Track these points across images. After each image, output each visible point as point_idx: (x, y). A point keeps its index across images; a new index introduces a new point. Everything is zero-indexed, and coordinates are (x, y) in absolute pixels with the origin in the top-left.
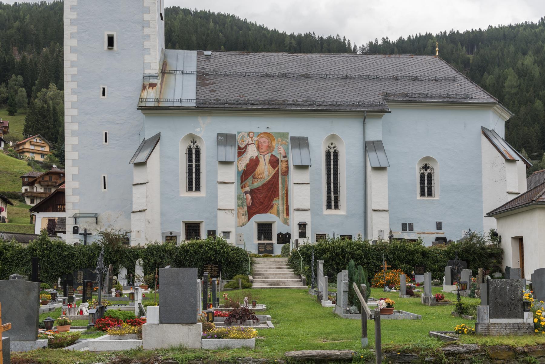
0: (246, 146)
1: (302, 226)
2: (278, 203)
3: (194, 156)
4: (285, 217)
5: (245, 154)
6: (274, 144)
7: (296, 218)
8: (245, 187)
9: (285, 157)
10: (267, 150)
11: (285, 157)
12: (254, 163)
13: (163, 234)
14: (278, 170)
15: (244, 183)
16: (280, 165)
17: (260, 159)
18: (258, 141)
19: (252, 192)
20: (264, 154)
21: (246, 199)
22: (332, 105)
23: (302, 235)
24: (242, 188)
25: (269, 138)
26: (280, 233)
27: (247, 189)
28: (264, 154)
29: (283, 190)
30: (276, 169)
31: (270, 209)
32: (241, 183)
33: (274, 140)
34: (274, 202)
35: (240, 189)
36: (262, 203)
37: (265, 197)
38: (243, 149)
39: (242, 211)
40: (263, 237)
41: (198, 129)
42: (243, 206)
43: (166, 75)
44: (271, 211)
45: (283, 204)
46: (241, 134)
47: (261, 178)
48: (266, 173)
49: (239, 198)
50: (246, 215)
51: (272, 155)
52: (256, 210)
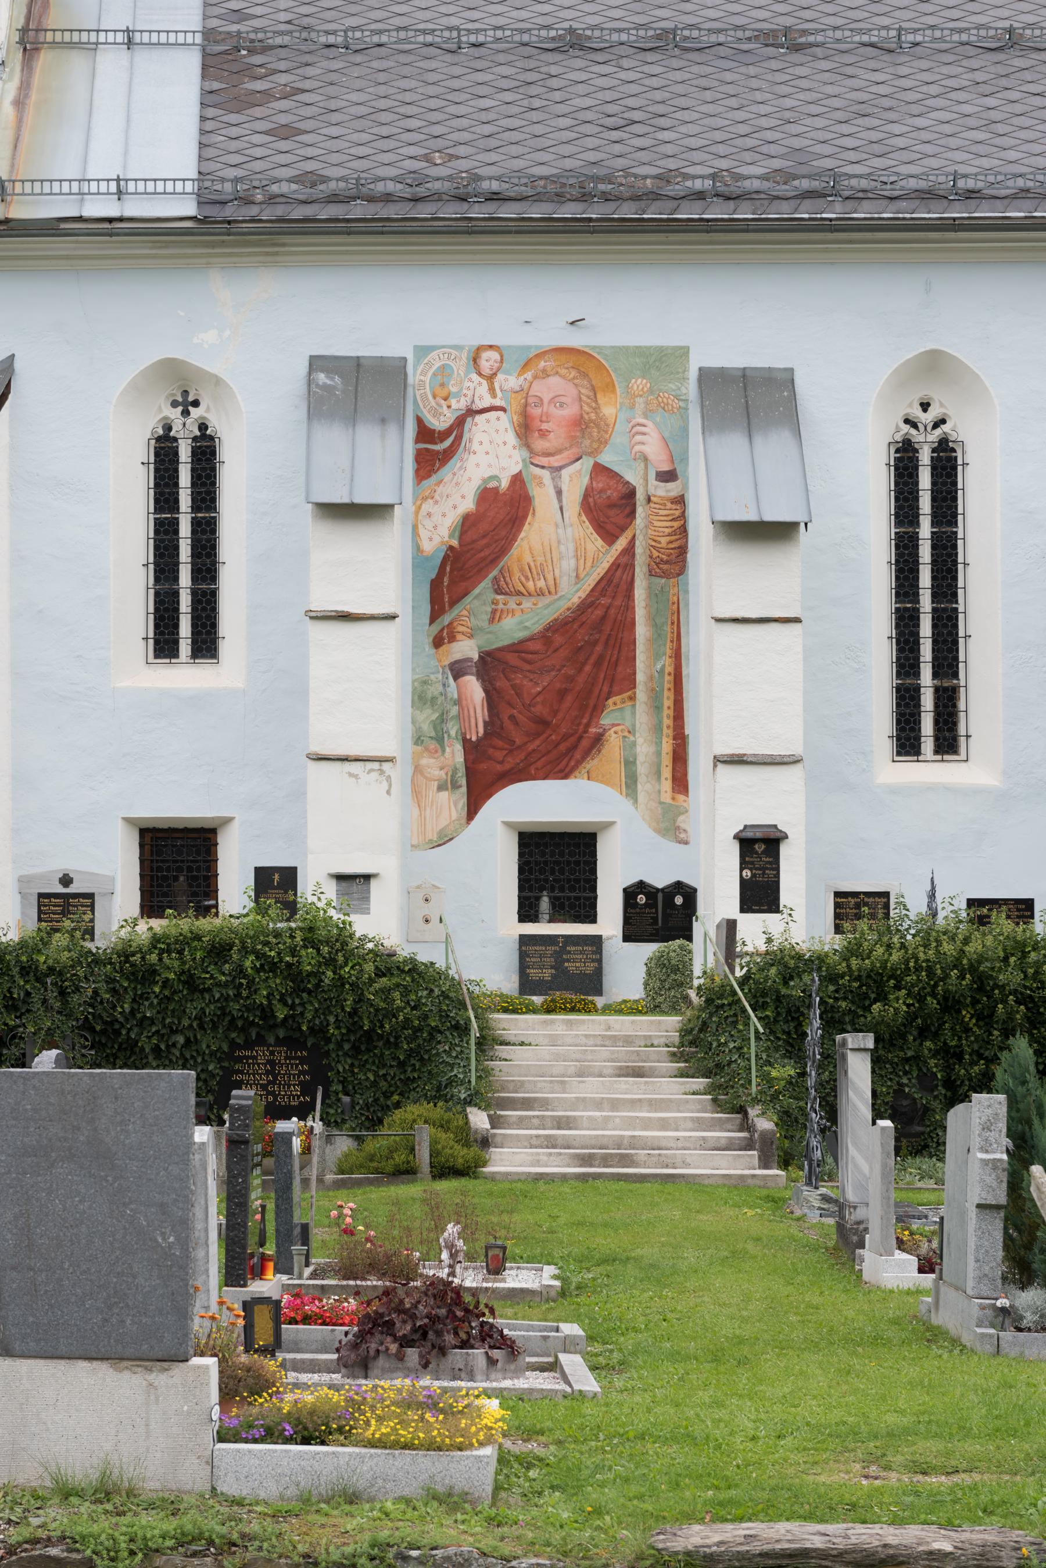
0: (460, 423)
1: (760, 849)
2: (630, 725)
3: (185, 478)
4: (667, 796)
5: (454, 463)
6: (608, 411)
7: (729, 803)
8: (452, 639)
9: (668, 476)
10: (573, 441)
11: (668, 476)
12: (502, 514)
13: (24, 881)
15: (446, 619)
17: (534, 491)
19: (490, 666)
20: (555, 461)
21: (459, 702)
22: (928, 195)
23: (760, 893)
24: (438, 642)
25: (585, 375)
26: (641, 886)
27: (466, 649)
28: (555, 461)
30: (621, 543)
31: (587, 753)
32: (433, 620)
33: (610, 387)
34: (605, 720)
35: (429, 650)
36: (543, 723)
37: (562, 694)
38: (447, 433)
39: (434, 768)
41: (210, 337)
42: (440, 739)
43: (44, 58)
44: (590, 764)
45: (657, 729)
47: (540, 593)
48: (568, 565)
49: (421, 698)
50: (455, 786)
51: (600, 470)
52: (510, 762)
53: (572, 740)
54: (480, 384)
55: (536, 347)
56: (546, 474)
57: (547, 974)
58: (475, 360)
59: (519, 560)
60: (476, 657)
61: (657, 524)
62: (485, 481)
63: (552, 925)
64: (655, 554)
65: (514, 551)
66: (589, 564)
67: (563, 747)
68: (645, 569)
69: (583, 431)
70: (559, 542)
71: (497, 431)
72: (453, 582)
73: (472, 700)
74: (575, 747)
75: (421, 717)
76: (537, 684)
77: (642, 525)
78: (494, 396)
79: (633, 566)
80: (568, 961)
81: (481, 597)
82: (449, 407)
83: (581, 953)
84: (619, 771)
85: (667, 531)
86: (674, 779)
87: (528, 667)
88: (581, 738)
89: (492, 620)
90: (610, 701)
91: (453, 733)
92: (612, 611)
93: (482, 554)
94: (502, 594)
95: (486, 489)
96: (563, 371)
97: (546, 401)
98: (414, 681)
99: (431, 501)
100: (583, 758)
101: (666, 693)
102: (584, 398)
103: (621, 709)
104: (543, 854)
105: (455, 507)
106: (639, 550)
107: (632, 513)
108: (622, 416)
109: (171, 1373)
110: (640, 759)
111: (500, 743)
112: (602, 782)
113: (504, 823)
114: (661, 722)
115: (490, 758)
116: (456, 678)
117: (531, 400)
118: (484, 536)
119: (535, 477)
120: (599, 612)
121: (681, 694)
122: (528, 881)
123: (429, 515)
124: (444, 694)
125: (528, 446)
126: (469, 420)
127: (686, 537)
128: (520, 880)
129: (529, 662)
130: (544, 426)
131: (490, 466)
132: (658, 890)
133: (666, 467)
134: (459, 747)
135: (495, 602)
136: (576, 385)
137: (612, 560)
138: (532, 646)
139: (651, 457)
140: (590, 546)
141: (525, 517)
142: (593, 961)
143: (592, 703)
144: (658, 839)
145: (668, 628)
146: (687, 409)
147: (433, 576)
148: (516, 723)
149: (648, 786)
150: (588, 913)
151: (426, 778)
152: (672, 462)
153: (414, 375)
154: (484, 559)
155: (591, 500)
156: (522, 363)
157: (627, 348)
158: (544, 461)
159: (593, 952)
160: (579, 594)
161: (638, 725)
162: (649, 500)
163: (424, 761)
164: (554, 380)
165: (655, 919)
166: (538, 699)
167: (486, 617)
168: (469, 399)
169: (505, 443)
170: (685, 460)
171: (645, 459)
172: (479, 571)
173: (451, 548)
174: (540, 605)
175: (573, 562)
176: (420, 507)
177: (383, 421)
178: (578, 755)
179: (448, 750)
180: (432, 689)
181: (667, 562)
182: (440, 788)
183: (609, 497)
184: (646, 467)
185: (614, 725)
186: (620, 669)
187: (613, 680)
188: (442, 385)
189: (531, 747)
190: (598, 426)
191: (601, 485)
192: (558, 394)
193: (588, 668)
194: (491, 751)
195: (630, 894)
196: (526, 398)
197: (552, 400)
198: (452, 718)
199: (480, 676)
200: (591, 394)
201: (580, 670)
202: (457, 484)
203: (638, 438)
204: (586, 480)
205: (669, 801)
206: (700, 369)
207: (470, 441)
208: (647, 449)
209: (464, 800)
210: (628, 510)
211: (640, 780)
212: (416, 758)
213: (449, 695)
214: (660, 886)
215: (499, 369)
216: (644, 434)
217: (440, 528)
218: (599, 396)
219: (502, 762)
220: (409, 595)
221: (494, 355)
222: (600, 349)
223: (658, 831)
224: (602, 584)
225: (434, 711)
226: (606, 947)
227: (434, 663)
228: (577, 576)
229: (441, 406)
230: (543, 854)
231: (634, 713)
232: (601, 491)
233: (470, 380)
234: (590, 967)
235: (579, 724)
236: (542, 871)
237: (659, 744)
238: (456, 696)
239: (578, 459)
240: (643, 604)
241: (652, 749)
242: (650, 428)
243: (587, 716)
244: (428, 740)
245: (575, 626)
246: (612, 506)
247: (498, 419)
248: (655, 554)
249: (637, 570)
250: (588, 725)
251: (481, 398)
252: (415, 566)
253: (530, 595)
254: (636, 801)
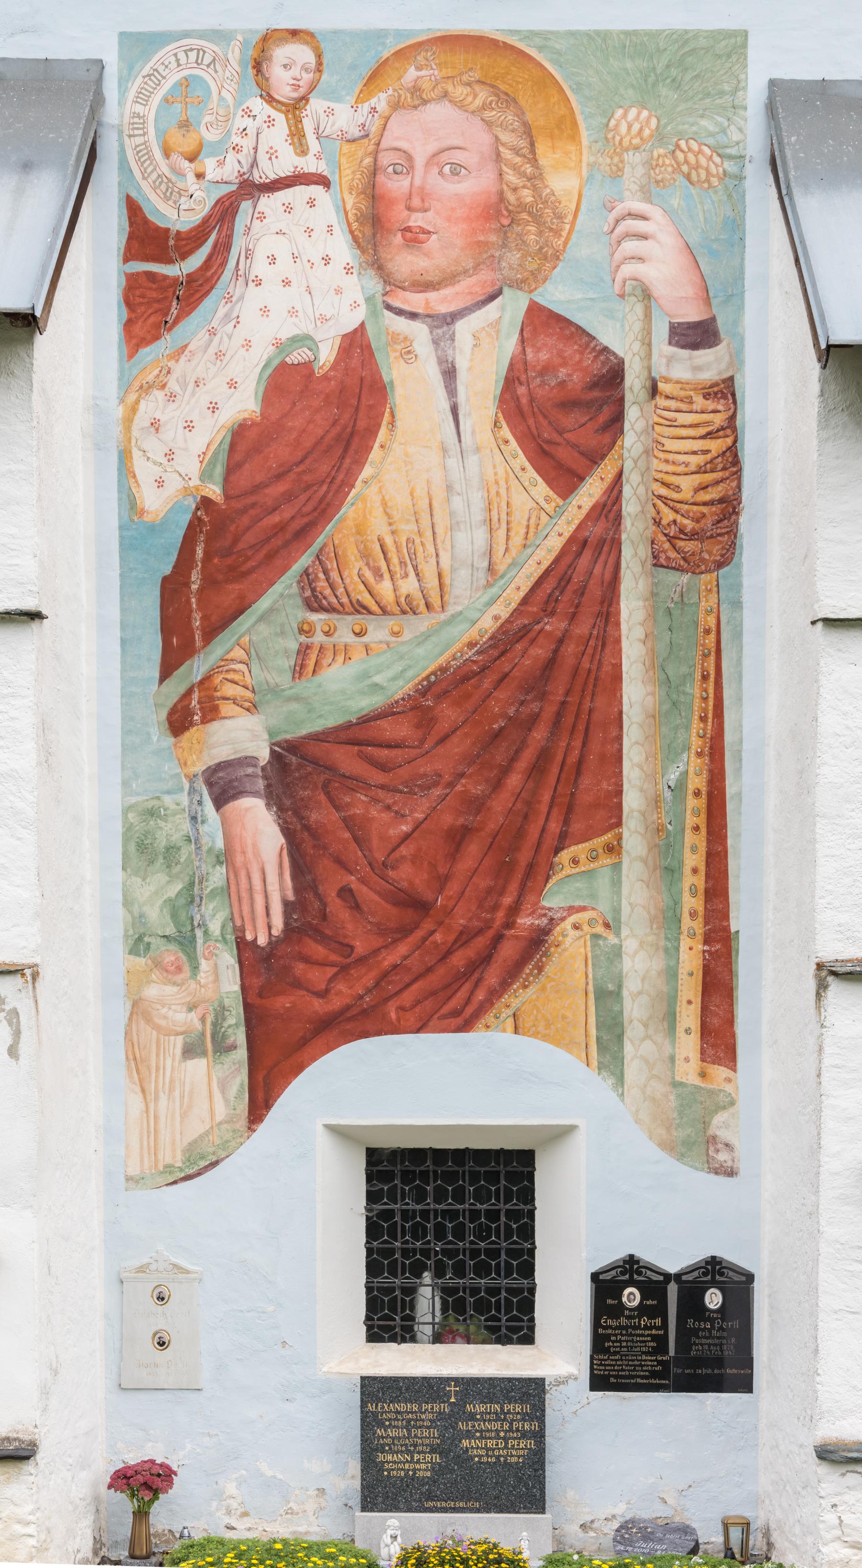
0: (225, 212)
2: (608, 907)
4: (688, 1071)
5: (212, 307)
6: (561, 183)
8: (211, 713)
9: (698, 335)
10: (482, 254)
11: (698, 335)
12: (325, 418)
14: (609, 509)
15: (197, 668)
17: (393, 370)
19: (297, 773)
20: (441, 301)
21: (226, 858)
24: (179, 722)
25: (508, 100)
26: (631, 1267)
27: (241, 736)
28: (441, 301)
30: (591, 491)
31: (513, 973)
33: (566, 127)
34: (554, 898)
35: (159, 736)
37: (457, 838)
38: (197, 236)
39: (176, 1006)
42: (185, 941)
44: (518, 998)
45: (669, 919)
46: (170, 67)
47: (408, 608)
48: (470, 541)
49: (143, 849)
50: (222, 1047)
51: (541, 321)
52: (344, 993)
53: (481, 942)
55: (399, 33)
56: (419, 332)
57: (424, 1465)
58: (258, 66)
59: (360, 530)
60: (264, 755)
61: (671, 445)
63: (441, 1349)
64: (668, 515)
65: (348, 511)
66: (517, 539)
67: (459, 960)
68: (644, 552)
69: (503, 231)
70: (449, 488)
71: (309, 231)
72: (209, 582)
73: (257, 854)
74: (486, 959)
76: (400, 816)
78: (302, 150)
80: (469, 1435)
81: (274, 615)
82: (200, 176)
83: (499, 1417)
84: (584, 1015)
85: (695, 461)
86: (706, 1031)
87: (380, 778)
88: (498, 938)
89: (299, 671)
90: (565, 856)
91: (215, 927)
92: (570, 649)
93: (276, 518)
94: (322, 609)
95: (283, 365)
96: (460, 92)
97: (419, 162)
98: (126, 811)
99: (159, 395)
100: (505, 985)
101: (689, 837)
102: (507, 154)
104: (421, 1197)
105: (214, 408)
106: (630, 506)
107: (615, 423)
108: (593, 197)
109: (205, 1535)
110: (631, 985)
111: (319, 951)
112: (545, 1038)
113: (327, 1126)
114: (677, 902)
115: (297, 984)
116: (220, 802)
117: (385, 159)
119: (395, 338)
120: (540, 652)
123: (155, 425)
124: (193, 840)
125: (379, 267)
126: (246, 206)
127: (738, 475)
128: (370, 1251)
129: (383, 767)
130: (417, 220)
131: (293, 312)
132: (668, 1277)
133: (692, 314)
134: (228, 960)
135: (305, 630)
136: (489, 124)
137: (567, 533)
138: (390, 730)
140: (522, 503)
141: (372, 431)
142: (524, 1435)
143: (524, 857)
144: (669, 1164)
145: (694, 689)
146: (741, 178)
148: (357, 907)
149: (648, 1047)
150: (510, 1317)
151: (158, 1028)
152: (707, 301)
153: (121, 103)
154: (281, 528)
155: (522, 390)
156: (366, 72)
157: (604, 36)
158: (415, 301)
159: (526, 1417)
160: (496, 610)
161: (625, 909)
162: (654, 391)
163: (152, 991)
164: (438, 113)
165: (661, 1343)
166: (404, 850)
169: (327, 260)
170: (735, 294)
171: (647, 295)
172: (270, 557)
173: (206, 503)
174: (407, 636)
175: (481, 536)
176: (134, 409)
177: (27, 166)
178: (492, 977)
179: (204, 965)
181: (693, 536)
182: (190, 1051)
183: (562, 384)
184: (648, 315)
185: (572, 910)
186: (586, 781)
187: (570, 809)
188: (185, 125)
189: (389, 959)
190: (537, 218)
191: (544, 356)
193: (514, 780)
194: (299, 968)
195: (605, 1288)
196: (376, 154)
198: (213, 894)
200: (523, 143)
201: (497, 785)
202: (220, 355)
203: (630, 246)
204: (510, 345)
205: (693, 1079)
206: (772, 83)
207: (249, 254)
208: (650, 273)
209: (243, 1077)
211: (629, 1034)
212: (134, 985)
213: (205, 841)
214: (673, 1268)
216: (644, 237)
217: (181, 465)
218: (540, 148)
219: (323, 994)
220: (114, 612)
221: (302, 54)
222: (543, 37)
223: (668, 1147)
224: (548, 587)
225: (172, 878)
226: (554, 1402)
227: (171, 768)
228: (491, 569)
229: (182, 174)
230: (421, 1197)
231: (616, 883)
232: (546, 369)
233: (249, 113)
234: (518, 1451)
235: (495, 908)
236: (418, 1232)
237: (672, 952)
238: (220, 844)
239: (492, 297)
240: (639, 632)
241: (657, 964)
242: (657, 223)
243: (513, 888)
244: (160, 943)
245: (487, 684)
246: (569, 404)
247: (311, 203)
248: (668, 515)
250: (514, 910)
251: (272, 154)
252: (127, 546)
253: (385, 612)
254: (620, 1079)
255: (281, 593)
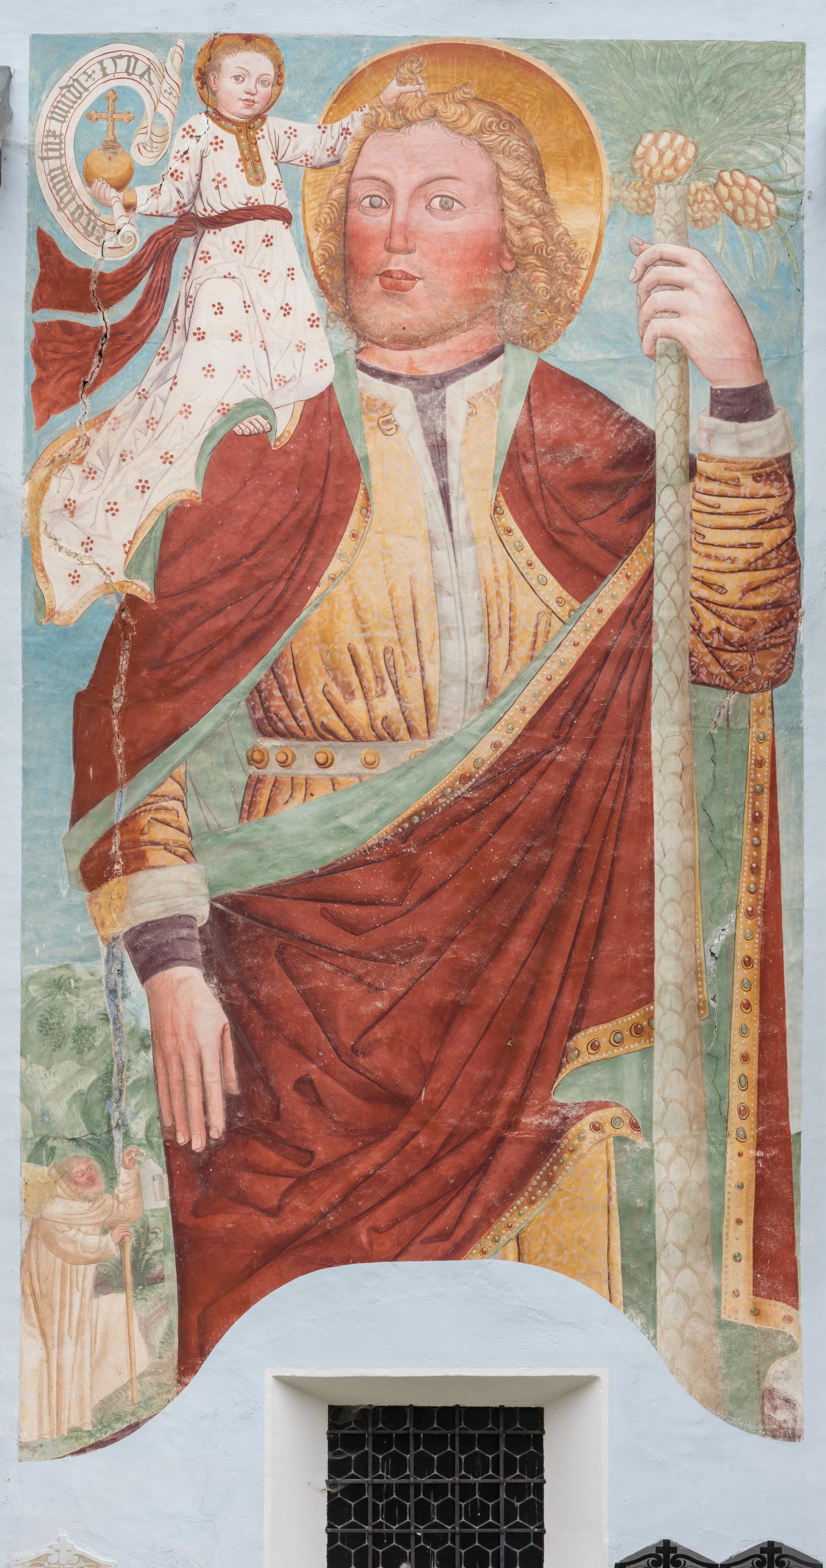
0: (160, 251)
4: (738, 1308)
5: (143, 365)
6: (578, 221)
8: (136, 861)
9: (746, 404)
10: (479, 305)
11: (746, 404)
12: (280, 504)
15: (119, 805)
16: (665, 529)
17: (368, 443)
18: (340, 167)
19: (242, 937)
20: (428, 361)
21: (153, 1040)
24: (95, 872)
25: (512, 122)
27: (176, 889)
28: (428, 361)
29: (713, 912)
30: (614, 592)
31: (515, 1187)
32: (81, 807)
33: (583, 155)
34: (568, 1092)
35: (69, 890)
37: (446, 1017)
38: (124, 280)
39: (84, 1227)
40: (385, 1490)
42: (100, 1145)
44: (523, 1216)
45: (712, 1118)
47: (385, 733)
48: (464, 652)
50: (145, 1279)
52: (301, 1211)
53: (475, 1147)
54: (217, 144)
55: (377, 41)
56: (401, 398)
58: (203, 77)
59: (326, 637)
61: (713, 536)
62: (227, 413)
64: (710, 622)
65: (311, 614)
66: (522, 650)
67: (448, 1168)
68: (680, 665)
69: (506, 277)
70: (438, 587)
71: (265, 275)
72: (135, 699)
73: (192, 1036)
74: (482, 1168)
75: (48, 1082)
76: (374, 990)
77: (672, 541)
78: (257, 178)
79: (646, 656)
81: (217, 741)
82: (129, 207)
84: (606, 1238)
85: (743, 556)
87: (349, 942)
88: (498, 1141)
89: (247, 810)
90: (582, 1039)
91: (138, 1128)
92: (588, 785)
93: (220, 622)
94: (277, 733)
95: (231, 436)
96: (452, 111)
97: (402, 194)
98: (26, 982)
99: (75, 471)
100: (506, 1200)
101: (738, 1017)
102: (510, 186)
103: (612, 1061)
104: (398, 1468)
105: (144, 487)
106: (663, 611)
107: (646, 506)
108: (615, 237)
110: (665, 1201)
111: (271, 1157)
112: (557, 1267)
113: (282, 1380)
114: (722, 1098)
115: (242, 1199)
116: (145, 972)
117: (359, 190)
118: (225, 571)
119: (370, 404)
120: (551, 787)
121: (780, 1018)
122: (355, 1491)
123: (70, 508)
125: (351, 318)
126: (186, 244)
128: (332, 1538)
129: (353, 929)
130: (398, 263)
131: (244, 372)
134: (154, 1169)
135: (256, 759)
136: (488, 150)
138: (362, 883)
139: (698, 350)
141: (343, 516)
143: (530, 1042)
145: (743, 834)
147: (83, 684)
148: (318, 1103)
149: (687, 1278)
151: (63, 1255)
152: (758, 363)
154: (227, 633)
155: (528, 469)
156: (337, 86)
157: (631, 47)
158: (396, 360)
160: (495, 735)
162: (692, 471)
163: (57, 1209)
164: (425, 135)
166: (378, 1032)
167: (233, 800)
168: (186, 188)
169: (286, 310)
171: (682, 356)
172: (212, 669)
173: (132, 603)
174: (384, 767)
175: (476, 645)
176: (43, 488)
178: (489, 1191)
179: (124, 1175)
180: (78, 1002)
181: (741, 646)
183: (579, 461)
184: (684, 380)
185: (591, 1107)
186: (608, 947)
187: (588, 982)
188: (112, 146)
189: (360, 1167)
190: (547, 263)
191: (556, 428)
192: (436, 173)
193: (518, 946)
194: (245, 1179)
196: (348, 184)
197: (419, 190)
198: (136, 1086)
199: (213, 968)
200: (530, 173)
201: (497, 951)
202: (151, 423)
203: (662, 297)
204: (514, 414)
205: (743, 1318)
209: (172, 1316)
210: (631, 500)
211: (662, 1260)
213: (127, 1020)
215: (270, 103)
216: (679, 286)
218: (553, 179)
219: (275, 1212)
221: (258, 64)
222: (555, 48)
223: (713, 1404)
224: (561, 708)
225: (84, 1066)
227: (84, 929)
228: (489, 686)
230: (398, 1468)
231: (647, 1073)
232: (558, 445)
233: (190, 133)
235: (494, 1104)
236: (394, 1512)
238: (145, 1023)
239: (492, 357)
240: (674, 764)
241: (698, 1174)
242: (696, 269)
243: (517, 1078)
245: (484, 826)
246: (586, 486)
247: (268, 241)
248: (710, 622)
249: (659, 667)
250: (518, 1106)
251: (220, 182)
252: (32, 655)
253: (356, 737)
254: (651, 1319)
255: (226, 715)
